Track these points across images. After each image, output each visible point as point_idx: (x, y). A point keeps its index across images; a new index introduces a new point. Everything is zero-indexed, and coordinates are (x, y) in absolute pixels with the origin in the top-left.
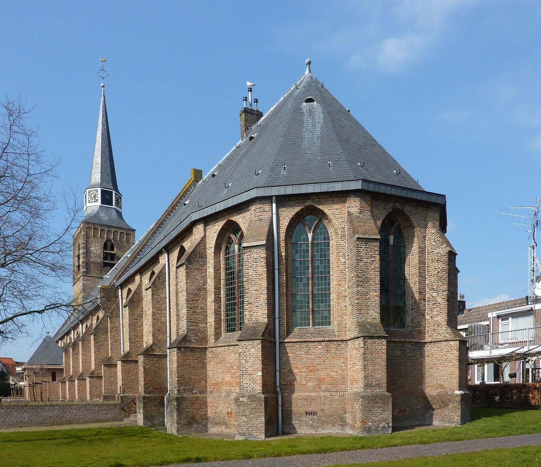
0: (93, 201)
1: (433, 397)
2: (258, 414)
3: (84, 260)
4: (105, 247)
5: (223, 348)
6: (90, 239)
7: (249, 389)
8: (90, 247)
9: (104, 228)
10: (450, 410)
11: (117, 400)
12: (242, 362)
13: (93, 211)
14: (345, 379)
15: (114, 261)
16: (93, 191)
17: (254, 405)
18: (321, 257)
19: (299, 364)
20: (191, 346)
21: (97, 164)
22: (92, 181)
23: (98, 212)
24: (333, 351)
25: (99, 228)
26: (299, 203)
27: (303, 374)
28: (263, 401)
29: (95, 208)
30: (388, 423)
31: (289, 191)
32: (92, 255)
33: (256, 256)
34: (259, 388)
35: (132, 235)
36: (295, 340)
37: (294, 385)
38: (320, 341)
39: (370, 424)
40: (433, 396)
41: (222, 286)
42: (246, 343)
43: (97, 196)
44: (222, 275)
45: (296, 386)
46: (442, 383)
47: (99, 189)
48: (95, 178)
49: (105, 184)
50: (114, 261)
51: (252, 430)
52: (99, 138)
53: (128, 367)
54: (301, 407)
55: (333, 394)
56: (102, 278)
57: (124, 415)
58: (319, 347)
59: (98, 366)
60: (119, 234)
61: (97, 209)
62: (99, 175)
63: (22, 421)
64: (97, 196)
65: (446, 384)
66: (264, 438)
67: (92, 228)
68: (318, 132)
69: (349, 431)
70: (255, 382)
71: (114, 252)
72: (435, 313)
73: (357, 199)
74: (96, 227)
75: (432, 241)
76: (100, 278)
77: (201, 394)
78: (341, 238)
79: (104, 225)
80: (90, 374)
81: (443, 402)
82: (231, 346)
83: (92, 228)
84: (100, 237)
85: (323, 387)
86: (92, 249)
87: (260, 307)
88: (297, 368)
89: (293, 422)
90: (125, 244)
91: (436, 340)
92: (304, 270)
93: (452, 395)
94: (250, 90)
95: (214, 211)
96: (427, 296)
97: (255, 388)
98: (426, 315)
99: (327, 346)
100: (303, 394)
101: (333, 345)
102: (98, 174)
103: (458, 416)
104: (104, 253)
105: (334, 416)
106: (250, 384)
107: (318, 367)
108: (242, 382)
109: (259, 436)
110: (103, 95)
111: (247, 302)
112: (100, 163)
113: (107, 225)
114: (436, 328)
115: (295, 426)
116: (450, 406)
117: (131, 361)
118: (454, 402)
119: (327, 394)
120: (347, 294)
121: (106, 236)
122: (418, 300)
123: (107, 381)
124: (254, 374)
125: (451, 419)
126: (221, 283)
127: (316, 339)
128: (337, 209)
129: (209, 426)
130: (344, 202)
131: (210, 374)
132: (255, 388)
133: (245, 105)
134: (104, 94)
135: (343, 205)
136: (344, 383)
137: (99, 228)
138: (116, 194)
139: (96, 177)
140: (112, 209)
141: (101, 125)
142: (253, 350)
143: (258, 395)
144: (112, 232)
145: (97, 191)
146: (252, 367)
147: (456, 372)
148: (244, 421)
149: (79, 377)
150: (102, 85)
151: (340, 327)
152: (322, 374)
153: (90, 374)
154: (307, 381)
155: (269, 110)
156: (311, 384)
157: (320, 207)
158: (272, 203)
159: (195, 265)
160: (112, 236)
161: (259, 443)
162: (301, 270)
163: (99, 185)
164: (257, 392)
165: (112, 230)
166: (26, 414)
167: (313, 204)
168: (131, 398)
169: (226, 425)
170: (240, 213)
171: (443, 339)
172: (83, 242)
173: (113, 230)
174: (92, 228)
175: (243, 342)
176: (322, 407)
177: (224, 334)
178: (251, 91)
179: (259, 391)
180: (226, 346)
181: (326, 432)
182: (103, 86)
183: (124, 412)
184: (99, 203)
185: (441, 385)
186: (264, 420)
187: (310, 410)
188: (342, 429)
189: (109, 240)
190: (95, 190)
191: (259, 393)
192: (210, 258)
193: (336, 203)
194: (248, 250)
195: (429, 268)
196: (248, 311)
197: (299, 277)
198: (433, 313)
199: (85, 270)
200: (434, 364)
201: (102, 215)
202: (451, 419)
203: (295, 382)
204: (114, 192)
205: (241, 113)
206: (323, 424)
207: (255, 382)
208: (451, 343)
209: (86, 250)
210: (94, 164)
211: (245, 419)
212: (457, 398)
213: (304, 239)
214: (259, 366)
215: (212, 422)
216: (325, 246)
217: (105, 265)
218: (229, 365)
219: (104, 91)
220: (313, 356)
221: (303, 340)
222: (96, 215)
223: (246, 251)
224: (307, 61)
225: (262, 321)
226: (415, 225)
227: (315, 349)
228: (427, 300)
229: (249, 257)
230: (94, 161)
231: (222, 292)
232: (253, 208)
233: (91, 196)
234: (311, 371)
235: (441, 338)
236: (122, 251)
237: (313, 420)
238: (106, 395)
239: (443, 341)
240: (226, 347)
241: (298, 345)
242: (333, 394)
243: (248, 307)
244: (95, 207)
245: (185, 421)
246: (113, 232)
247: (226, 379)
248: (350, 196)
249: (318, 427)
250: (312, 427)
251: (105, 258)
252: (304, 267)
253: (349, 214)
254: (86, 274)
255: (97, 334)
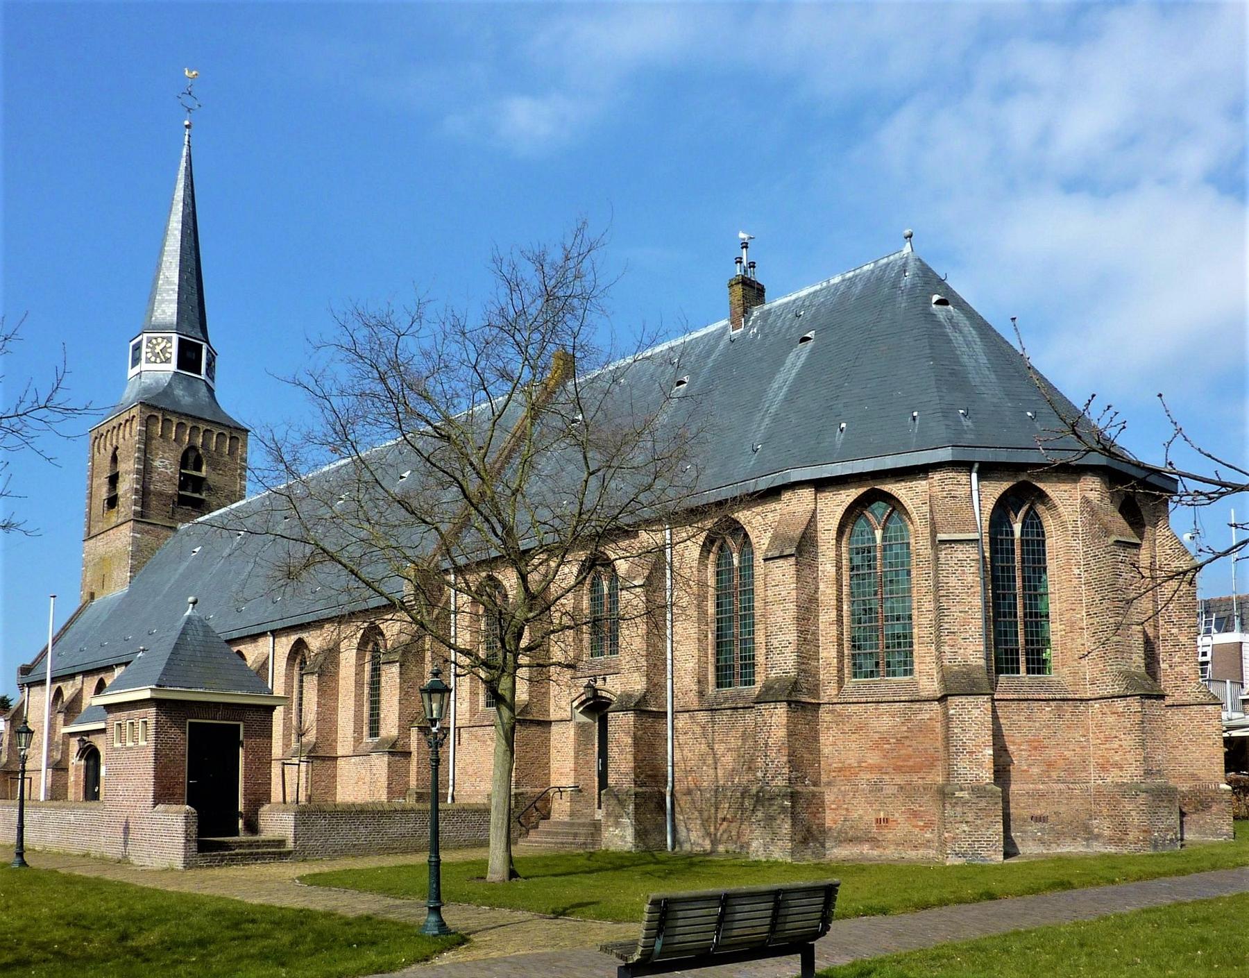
0: (158, 360)
1: (1182, 794)
2: (990, 819)
3: (138, 487)
4: (184, 463)
5: (863, 705)
6: (154, 441)
7: (969, 777)
8: (152, 460)
9: (183, 421)
10: (1214, 814)
11: (449, 800)
12: (956, 731)
13: (157, 383)
14: (1087, 763)
15: (201, 494)
16: (160, 340)
17: (983, 804)
18: (1034, 563)
19: (1018, 737)
20: (803, 700)
21: (168, 282)
22: (156, 319)
23: (170, 384)
24: (1068, 715)
25: (175, 420)
26: (1009, 475)
27: (1023, 753)
28: (999, 797)
29: (162, 376)
30: (1176, 834)
31: (1003, 456)
32: (155, 477)
33: (961, 556)
34: (988, 775)
35: (240, 440)
36: (1011, 697)
37: (1009, 771)
38: (1049, 700)
39: (1156, 834)
40: (1183, 792)
41: (844, 597)
42: (963, 699)
43: (169, 350)
44: (844, 578)
45: (1012, 773)
46: (1196, 772)
47: (175, 337)
48: (164, 312)
49: (186, 328)
50: (201, 494)
51: (979, 847)
52: (176, 229)
53: (525, 733)
54: (1023, 808)
55: (1071, 786)
56: (173, 529)
57: (519, 832)
58: (1047, 709)
59: (404, 729)
60: (215, 437)
61: (168, 380)
62: (174, 307)
63: (355, 845)
64: (169, 350)
65: (1202, 774)
66: (1002, 859)
67: (158, 419)
68: (983, 360)
69: (1098, 848)
70: (980, 765)
71: (203, 474)
72: (1176, 659)
73: (1097, 480)
74: (168, 417)
75: (1166, 547)
76: (171, 528)
77: (814, 786)
78: (1072, 537)
79: (186, 415)
80: (390, 748)
81: (1201, 802)
82: (882, 702)
83: (160, 418)
84: (175, 440)
85: (1054, 775)
86: (157, 463)
87: (971, 640)
88: (1014, 743)
89: (1013, 835)
90: (227, 458)
91: (1181, 702)
92: (1009, 581)
93: (1217, 790)
94: (745, 246)
95: (849, 472)
96: (1161, 633)
97: (981, 775)
98: (1161, 662)
99: (1059, 708)
100: (1026, 786)
101: (1067, 707)
102: (171, 305)
103: (1228, 825)
104: (181, 474)
105: (1075, 824)
106: (971, 768)
107: (1046, 742)
108: (957, 765)
109: (993, 857)
110: (186, 143)
111: (946, 631)
112: (177, 281)
113: (191, 416)
114: (1179, 683)
115: (1016, 841)
116: (1214, 808)
117: (532, 721)
118: (1221, 802)
119: (1062, 786)
120: (1084, 625)
121: (187, 438)
122: (1152, 638)
123: (422, 763)
124: (979, 752)
125: (1216, 830)
126: (842, 592)
127: (1042, 696)
128: (1065, 491)
129: (828, 845)
130: (1076, 481)
131: (826, 750)
132: (981, 775)
133: (738, 271)
134: (189, 142)
135: (1073, 485)
136: (1085, 769)
137: (175, 420)
138: (208, 351)
139: (167, 308)
140: (199, 381)
141: (182, 204)
142: (976, 712)
143: (988, 787)
144: (202, 431)
145: (169, 340)
146: (974, 740)
147: (1218, 754)
148: (965, 831)
149: (310, 751)
150: (187, 123)
151: (1077, 678)
152: (1052, 753)
153: (390, 748)
154: (1029, 766)
155: (794, 290)
156: (1035, 770)
157: (1040, 485)
158: (971, 473)
159: (805, 560)
160: (201, 440)
161: (996, 868)
162: (1003, 581)
163: (175, 327)
164: (984, 782)
165: (200, 426)
166: (362, 829)
167: (1029, 479)
168: (530, 797)
169: (874, 841)
170: (902, 480)
171: (1192, 702)
172: (139, 448)
173: (203, 427)
174: (160, 418)
175: (956, 698)
176: (1056, 808)
177: (850, 682)
178: (747, 247)
179: (988, 781)
180: (870, 702)
181: (1063, 851)
182: (188, 127)
183: (519, 826)
184: (173, 366)
185: (1193, 775)
186: (1002, 830)
187: (1038, 812)
188: (1088, 846)
189: (192, 448)
190: (163, 338)
191: (987, 784)
192: (825, 547)
193: (1064, 481)
194: (948, 545)
195: (1163, 590)
196: (949, 646)
197: (1001, 592)
198: (1174, 660)
199: (139, 509)
200: (1180, 740)
201: (179, 392)
202: (1216, 830)
203: (1011, 767)
204: (205, 346)
205: (734, 283)
206: (1059, 836)
207: (980, 765)
208: (1208, 708)
209: (145, 466)
210: (160, 282)
211: (966, 829)
212: (1225, 796)
213: (1007, 531)
214: (987, 738)
215: (837, 838)
216: (1038, 545)
217: (183, 501)
218: (877, 736)
219: (189, 136)
220: (1037, 724)
221: (1022, 697)
222: (167, 391)
223: (943, 547)
224: (907, 232)
225: (974, 664)
226: (1146, 523)
227: (1041, 712)
228: (1161, 638)
229: (949, 556)
230: (161, 277)
231: (294, 697)
232: (937, 476)
233: (153, 348)
234: (1035, 748)
235: (1190, 699)
236: (219, 474)
237: (1042, 830)
238: (421, 791)
239: (1193, 705)
240: (869, 705)
241: (1014, 705)
242: (1071, 786)
243: (950, 639)
244: (164, 375)
245: (800, 837)
246: (204, 432)
247: (870, 761)
248: (1086, 474)
249: (1051, 843)
250: (1042, 841)
251: (182, 486)
252: (1029, 582)
253: (1086, 501)
254: (142, 517)
255: (407, 664)
